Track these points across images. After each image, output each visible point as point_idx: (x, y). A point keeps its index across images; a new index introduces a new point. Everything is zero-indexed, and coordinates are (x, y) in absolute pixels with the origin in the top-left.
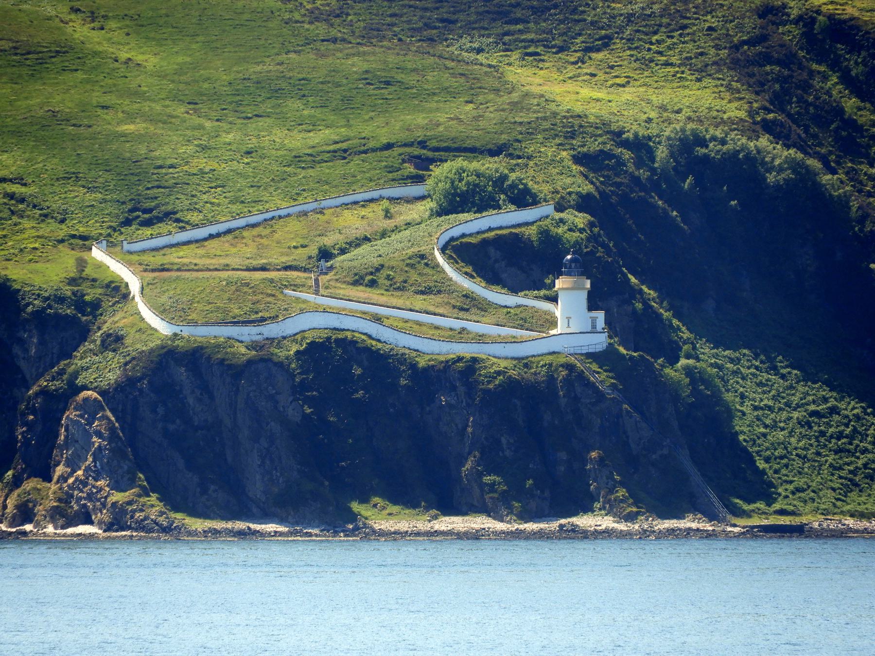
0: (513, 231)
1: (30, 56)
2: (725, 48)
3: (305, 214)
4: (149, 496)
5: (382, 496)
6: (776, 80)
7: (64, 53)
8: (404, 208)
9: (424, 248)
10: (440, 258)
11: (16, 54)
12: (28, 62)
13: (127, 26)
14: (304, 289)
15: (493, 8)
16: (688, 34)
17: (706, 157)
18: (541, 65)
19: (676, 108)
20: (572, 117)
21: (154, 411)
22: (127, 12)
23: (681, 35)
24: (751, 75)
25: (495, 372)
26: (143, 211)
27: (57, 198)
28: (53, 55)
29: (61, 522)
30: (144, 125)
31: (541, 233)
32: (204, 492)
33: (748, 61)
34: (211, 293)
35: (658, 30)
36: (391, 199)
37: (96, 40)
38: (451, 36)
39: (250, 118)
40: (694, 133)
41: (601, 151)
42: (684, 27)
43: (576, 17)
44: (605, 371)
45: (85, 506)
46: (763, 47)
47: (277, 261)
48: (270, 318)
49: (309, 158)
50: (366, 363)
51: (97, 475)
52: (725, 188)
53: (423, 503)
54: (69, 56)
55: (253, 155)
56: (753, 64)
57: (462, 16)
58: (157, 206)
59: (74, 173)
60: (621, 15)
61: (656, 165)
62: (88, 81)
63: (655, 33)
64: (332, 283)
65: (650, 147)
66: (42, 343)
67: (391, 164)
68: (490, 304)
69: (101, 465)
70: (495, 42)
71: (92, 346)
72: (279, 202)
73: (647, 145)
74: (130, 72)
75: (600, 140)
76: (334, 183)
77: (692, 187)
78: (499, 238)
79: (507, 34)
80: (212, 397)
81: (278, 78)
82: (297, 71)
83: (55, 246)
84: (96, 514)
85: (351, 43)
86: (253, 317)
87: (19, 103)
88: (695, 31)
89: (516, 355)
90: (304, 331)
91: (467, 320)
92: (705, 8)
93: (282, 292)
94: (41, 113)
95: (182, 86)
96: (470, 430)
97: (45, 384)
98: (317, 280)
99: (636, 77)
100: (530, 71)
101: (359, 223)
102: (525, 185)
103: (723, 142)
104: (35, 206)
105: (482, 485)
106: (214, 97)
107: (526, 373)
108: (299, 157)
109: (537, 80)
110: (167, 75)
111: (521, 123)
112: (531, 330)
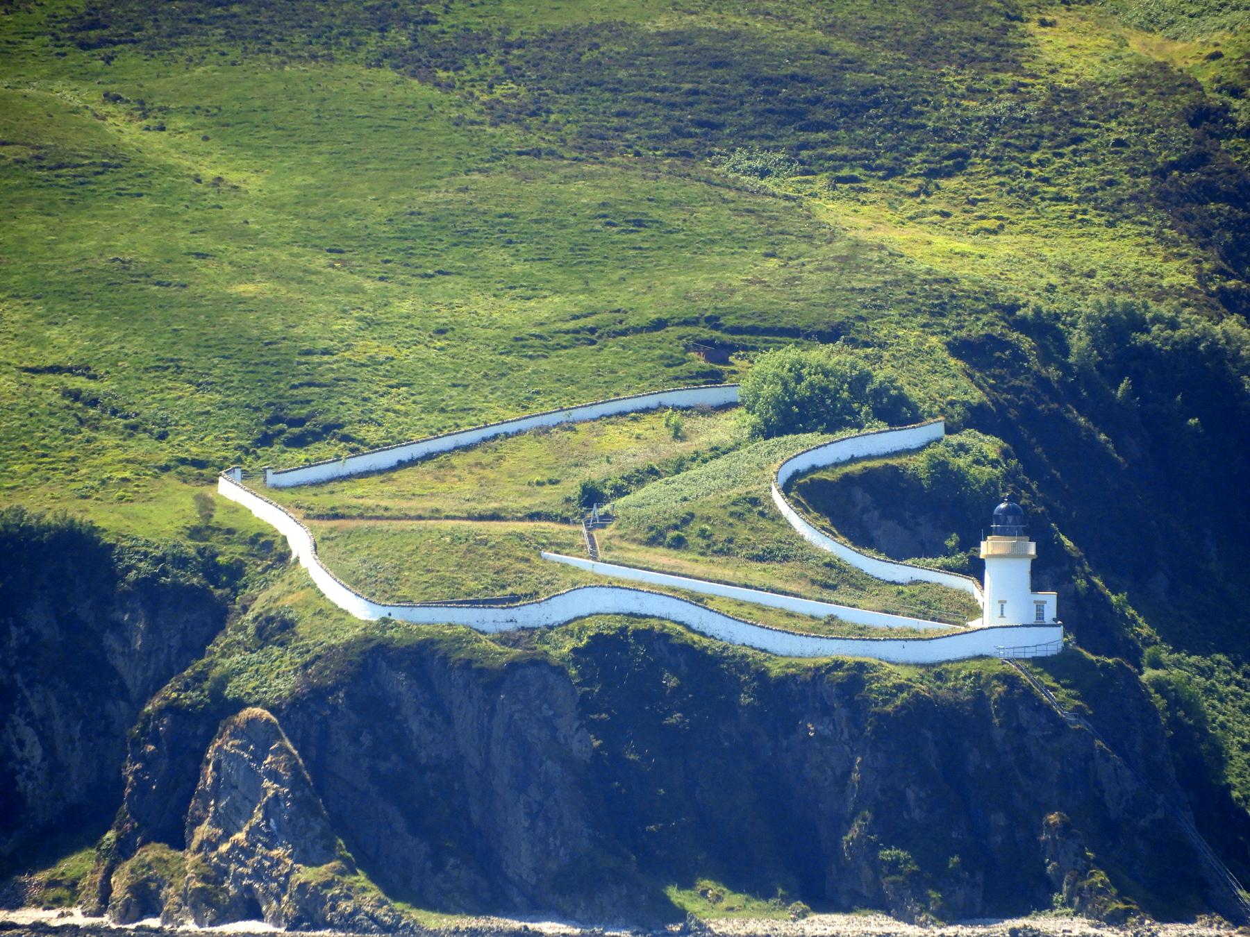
0: (890, 462)
1: (63, 171)
2: (1145, 174)
3: (544, 430)
4: (356, 874)
5: (716, 878)
6: (1226, 226)
7: (116, 167)
8: (700, 423)
9: (755, 488)
10: (781, 504)
11: (41, 168)
12: (62, 181)
13: (203, 126)
14: (574, 550)
15: (778, 105)
16: (1086, 151)
17: (1147, 346)
18: (862, 197)
19: (1086, 270)
20: (936, 281)
21: (355, 740)
22: (198, 103)
23: (1074, 152)
24: (1189, 218)
25: (894, 686)
26: (288, 423)
27: (148, 400)
28: (99, 170)
29: (209, 915)
30: (268, 285)
31: (934, 467)
32: (439, 867)
33: (1182, 196)
34: (428, 555)
35: (1038, 143)
36: (686, 410)
37: (157, 146)
38: (717, 150)
39: (431, 276)
40: (1128, 309)
41: (988, 336)
42: (1077, 140)
43: (910, 121)
44: (1065, 686)
45: (249, 888)
46: (1203, 174)
47: (515, 506)
48: (526, 595)
49: (537, 342)
50: (684, 669)
51: (271, 840)
52: (1179, 397)
53: (780, 891)
54: (123, 173)
55: (448, 335)
56: (1189, 200)
57: (730, 117)
58: (311, 415)
59: (172, 360)
60: (979, 119)
61: (1071, 360)
62: (162, 213)
63: (1034, 148)
64: (616, 542)
65: (1059, 332)
66: (153, 629)
67: (669, 353)
68: (869, 578)
69: (278, 824)
70: (788, 160)
71: (241, 637)
72: (502, 411)
73: (1054, 327)
74: (225, 199)
75: (985, 319)
76: (584, 382)
77: (1130, 395)
78: (869, 473)
79: (804, 146)
80: (449, 720)
81: (465, 213)
82: (494, 201)
83: (156, 477)
84: (269, 903)
85: (562, 157)
86: (499, 594)
87: (63, 247)
88: (1095, 146)
89: (921, 660)
90: (582, 618)
91: (837, 603)
92: (1105, 109)
93: (539, 555)
94: (102, 263)
95: (313, 224)
96: (855, 776)
97: (174, 695)
98: (591, 537)
99: (1013, 219)
100: (849, 207)
101: (634, 447)
102: (900, 389)
103: (1173, 325)
104: (114, 412)
105: (876, 865)
106: (368, 241)
107: (939, 688)
108: (522, 339)
109: (863, 222)
110: (284, 205)
111: (862, 291)
112: (940, 621)
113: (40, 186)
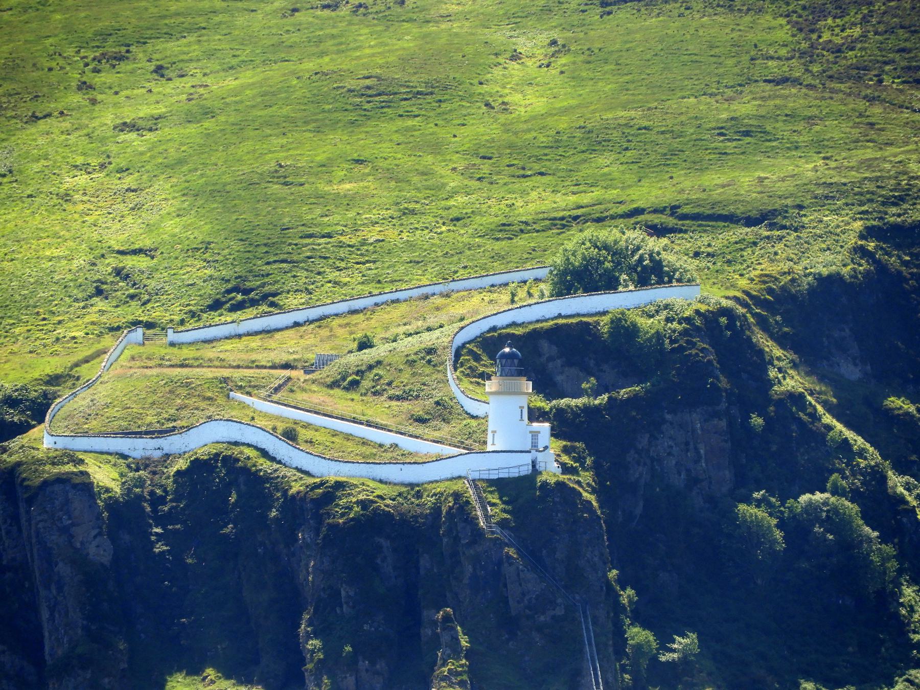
5: (218, 668)
113: (800, 157)
